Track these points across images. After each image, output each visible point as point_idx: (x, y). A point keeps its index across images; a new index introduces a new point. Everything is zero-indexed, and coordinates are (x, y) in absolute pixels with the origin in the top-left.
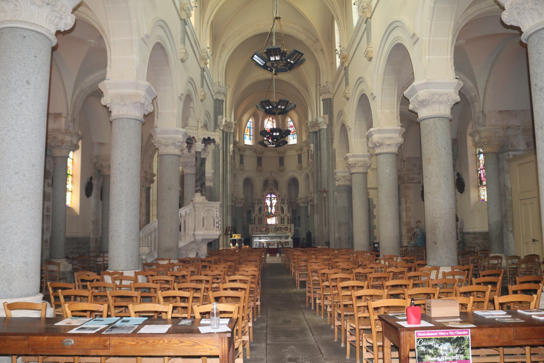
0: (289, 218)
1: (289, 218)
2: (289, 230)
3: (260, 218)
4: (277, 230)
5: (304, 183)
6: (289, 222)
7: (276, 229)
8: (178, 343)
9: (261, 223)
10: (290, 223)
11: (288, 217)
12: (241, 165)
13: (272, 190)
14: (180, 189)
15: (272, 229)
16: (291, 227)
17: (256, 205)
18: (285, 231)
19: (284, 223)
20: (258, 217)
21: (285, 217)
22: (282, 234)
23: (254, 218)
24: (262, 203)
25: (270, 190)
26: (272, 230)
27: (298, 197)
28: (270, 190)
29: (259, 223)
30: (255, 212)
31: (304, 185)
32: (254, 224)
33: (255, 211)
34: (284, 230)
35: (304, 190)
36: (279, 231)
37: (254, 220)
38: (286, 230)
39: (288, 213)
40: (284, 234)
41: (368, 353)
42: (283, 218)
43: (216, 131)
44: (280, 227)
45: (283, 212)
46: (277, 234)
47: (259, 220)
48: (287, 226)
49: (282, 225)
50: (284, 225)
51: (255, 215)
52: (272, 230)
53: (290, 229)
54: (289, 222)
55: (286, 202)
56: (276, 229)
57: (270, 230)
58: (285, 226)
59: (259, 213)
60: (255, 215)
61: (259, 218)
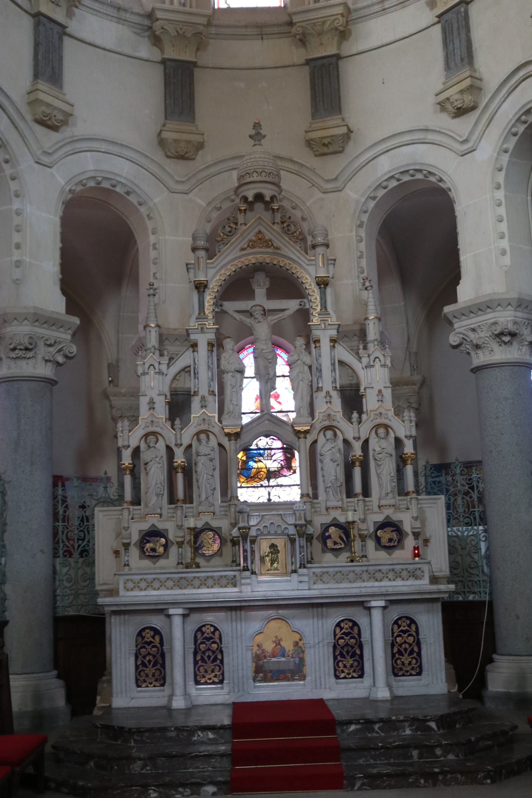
0: (409, 448)
1: (409, 448)
2: (410, 542)
3: (180, 459)
4: (317, 545)
5: (500, 195)
6: (410, 486)
7: (310, 538)
8: (254, 308)
9: (189, 499)
10: (417, 492)
11: (398, 442)
12: (42, 85)
13: (268, 244)
14: (412, 716)
15: (280, 542)
16: (420, 518)
17: (152, 358)
18: (382, 554)
19: (366, 492)
20: (161, 445)
21: (373, 444)
22: (359, 577)
23: (136, 452)
24: (194, 346)
25: (252, 245)
26: (273, 546)
27: (454, 299)
28: (252, 245)
29: (172, 499)
30: (144, 413)
31: (502, 211)
32: (137, 501)
33: (144, 402)
34: (371, 544)
35: (505, 244)
36: (329, 556)
37: (134, 472)
38: (389, 548)
39: (398, 412)
40: (373, 577)
41: (112, 556)
42: (358, 452)
43: (36, 366)
44: (336, 524)
45: (361, 412)
46: (320, 578)
47: (172, 470)
48: (396, 517)
49: (357, 502)
50: (367, 510)
51: (139, 432)
52: (273, 546)
53: (416, 535)
54: (410, 486)
55: (373, 332)
56: (310, 538)
57: (264, 547)
58: (380, 518)
59: (172, 418)
60: (139, 432)
61: (169, 450)
